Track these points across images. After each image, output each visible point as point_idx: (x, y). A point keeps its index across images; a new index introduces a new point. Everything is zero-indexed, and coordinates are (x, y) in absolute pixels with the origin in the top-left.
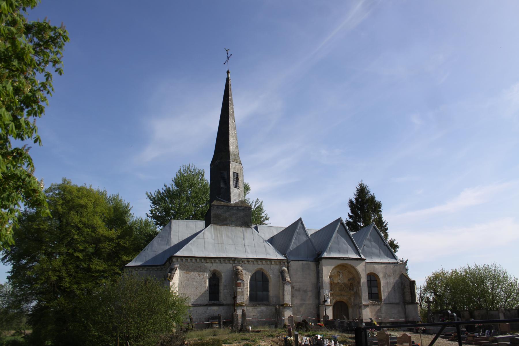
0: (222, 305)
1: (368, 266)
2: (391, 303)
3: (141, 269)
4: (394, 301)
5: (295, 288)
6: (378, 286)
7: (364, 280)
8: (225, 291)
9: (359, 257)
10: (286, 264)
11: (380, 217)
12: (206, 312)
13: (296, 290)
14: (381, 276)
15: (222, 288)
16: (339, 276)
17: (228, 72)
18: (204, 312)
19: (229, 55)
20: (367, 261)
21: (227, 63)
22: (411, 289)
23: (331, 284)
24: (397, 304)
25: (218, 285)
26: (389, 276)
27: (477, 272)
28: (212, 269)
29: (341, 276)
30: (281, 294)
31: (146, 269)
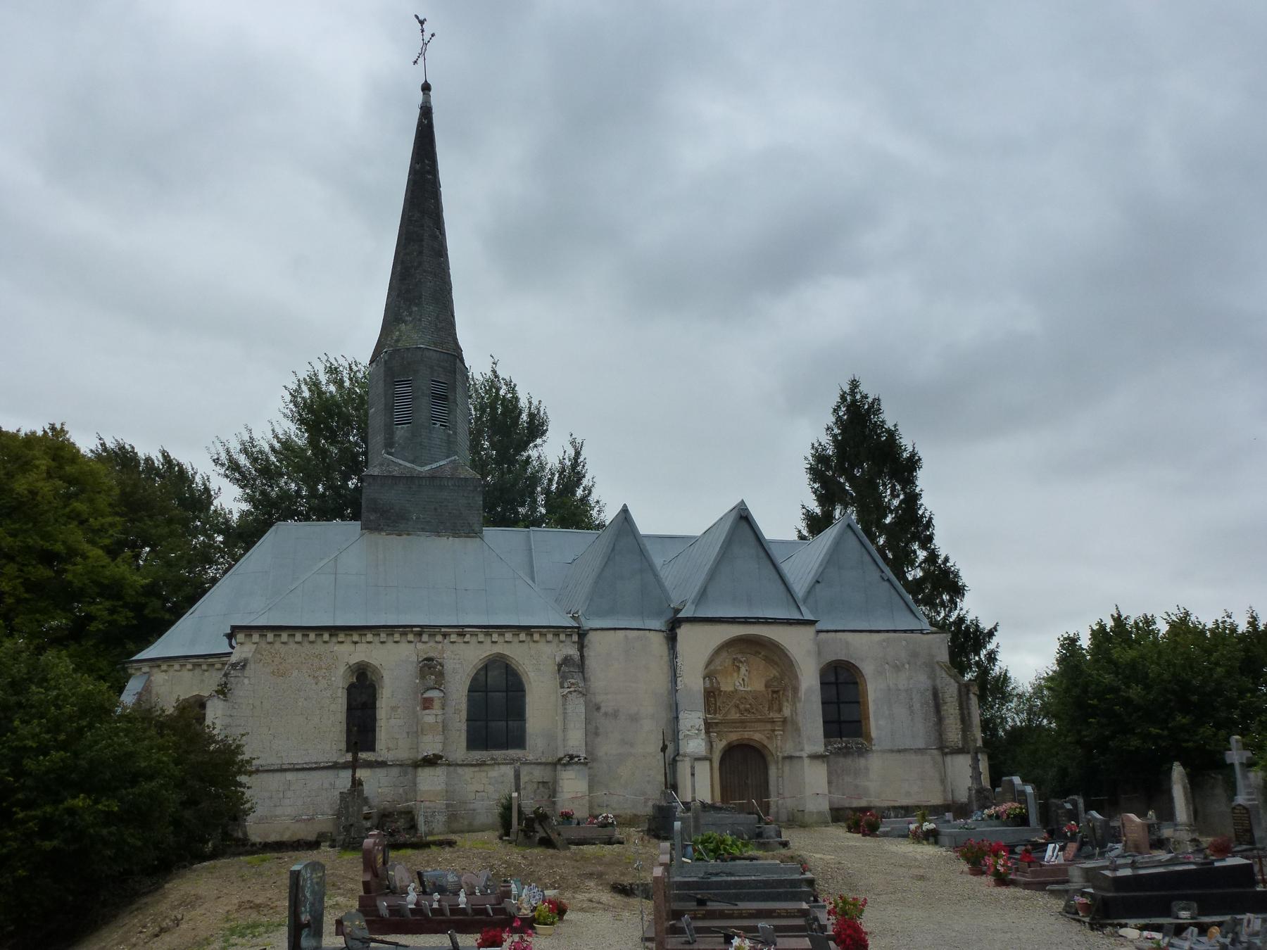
0: (382, 764)
1: (822, 635)
2: (899, 751)
3: (177, 667)
4: (908, 744)
5: (603, 710)
6: (858, 701)
7: (809, 679)
8: (393, 721)
9: (798, 617)
10: (575, 638)
11: (912, 499)
12: (333, 786)
13: (606, 714)
14: (867, 669)
15: (382, 712)
16: (739, 668)
17: (426, 88)
18: (326, 785)
19: (427, 36)
20: (819, 626)
21: (421, 59)
22: (961, 708)
23: (711, 696)
24: (919, 751)
25: (373, 707)
26: (898, 668)
27: (248, 806)
28: (354, 660)
29: (743, 670)
30: (560, 724)
31: (189, 666)
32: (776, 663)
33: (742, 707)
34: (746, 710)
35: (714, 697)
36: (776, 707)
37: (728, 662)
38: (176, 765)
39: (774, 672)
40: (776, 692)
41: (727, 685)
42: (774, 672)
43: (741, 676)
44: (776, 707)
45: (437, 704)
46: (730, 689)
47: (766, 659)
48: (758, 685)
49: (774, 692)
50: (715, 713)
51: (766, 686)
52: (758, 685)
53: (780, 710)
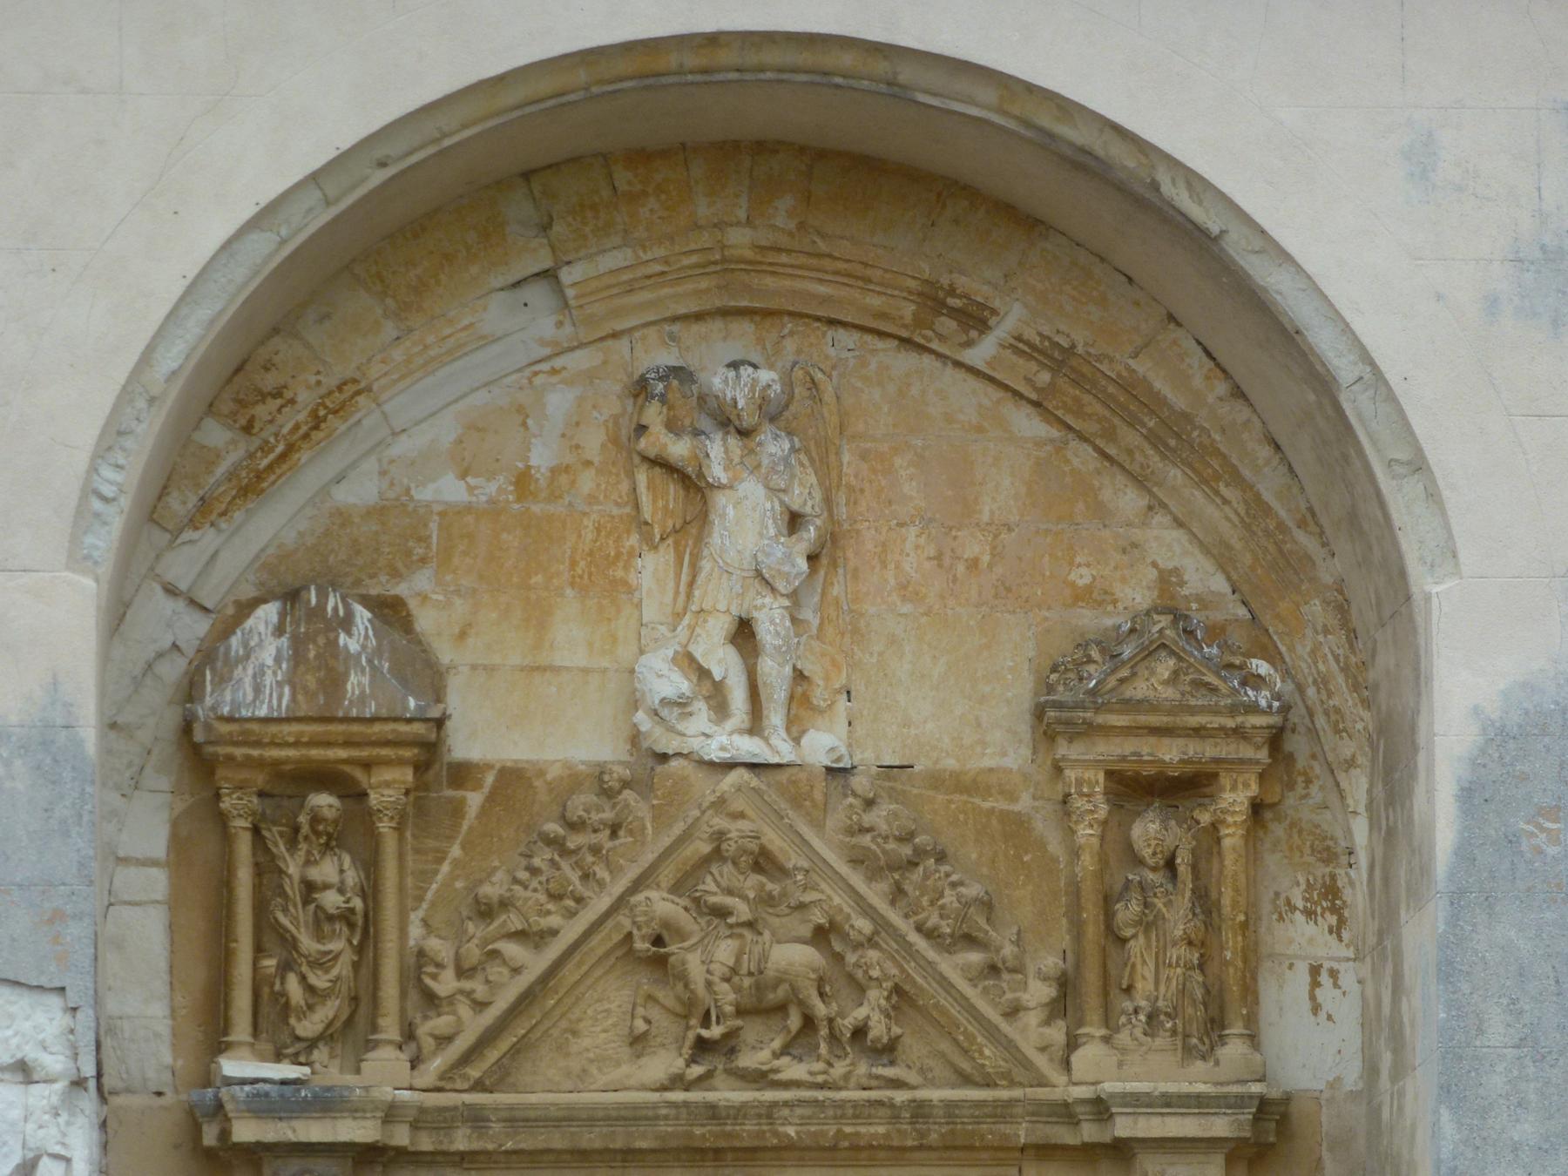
16: (692, 484)
29: (745, 520)
32: (1174, 434)
33: (708, 960)
34: (765, 1002)
35: (354, 832)
36: (1153, 975)
37: (566, 423)
38: (1550, 1117)
39: (1158, 551)
40: (1182, 789)
41: (538, 698)
42: (1158, 551)
43: (722, 598)
44: (1153, 975)
45: (1335, 965)
46: (569, 738)
47: (1062, 383)
48: (937, 697)
49: (1135, 789)
50: (353, 1032)
51: (1053, 722)
52: (937, 697)
53: (1218, 1009)
